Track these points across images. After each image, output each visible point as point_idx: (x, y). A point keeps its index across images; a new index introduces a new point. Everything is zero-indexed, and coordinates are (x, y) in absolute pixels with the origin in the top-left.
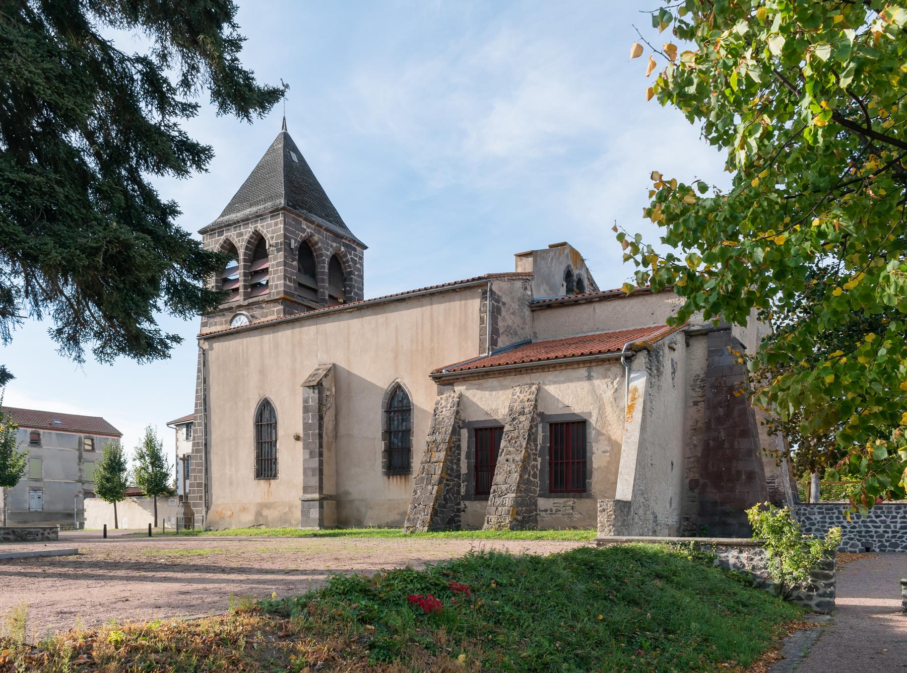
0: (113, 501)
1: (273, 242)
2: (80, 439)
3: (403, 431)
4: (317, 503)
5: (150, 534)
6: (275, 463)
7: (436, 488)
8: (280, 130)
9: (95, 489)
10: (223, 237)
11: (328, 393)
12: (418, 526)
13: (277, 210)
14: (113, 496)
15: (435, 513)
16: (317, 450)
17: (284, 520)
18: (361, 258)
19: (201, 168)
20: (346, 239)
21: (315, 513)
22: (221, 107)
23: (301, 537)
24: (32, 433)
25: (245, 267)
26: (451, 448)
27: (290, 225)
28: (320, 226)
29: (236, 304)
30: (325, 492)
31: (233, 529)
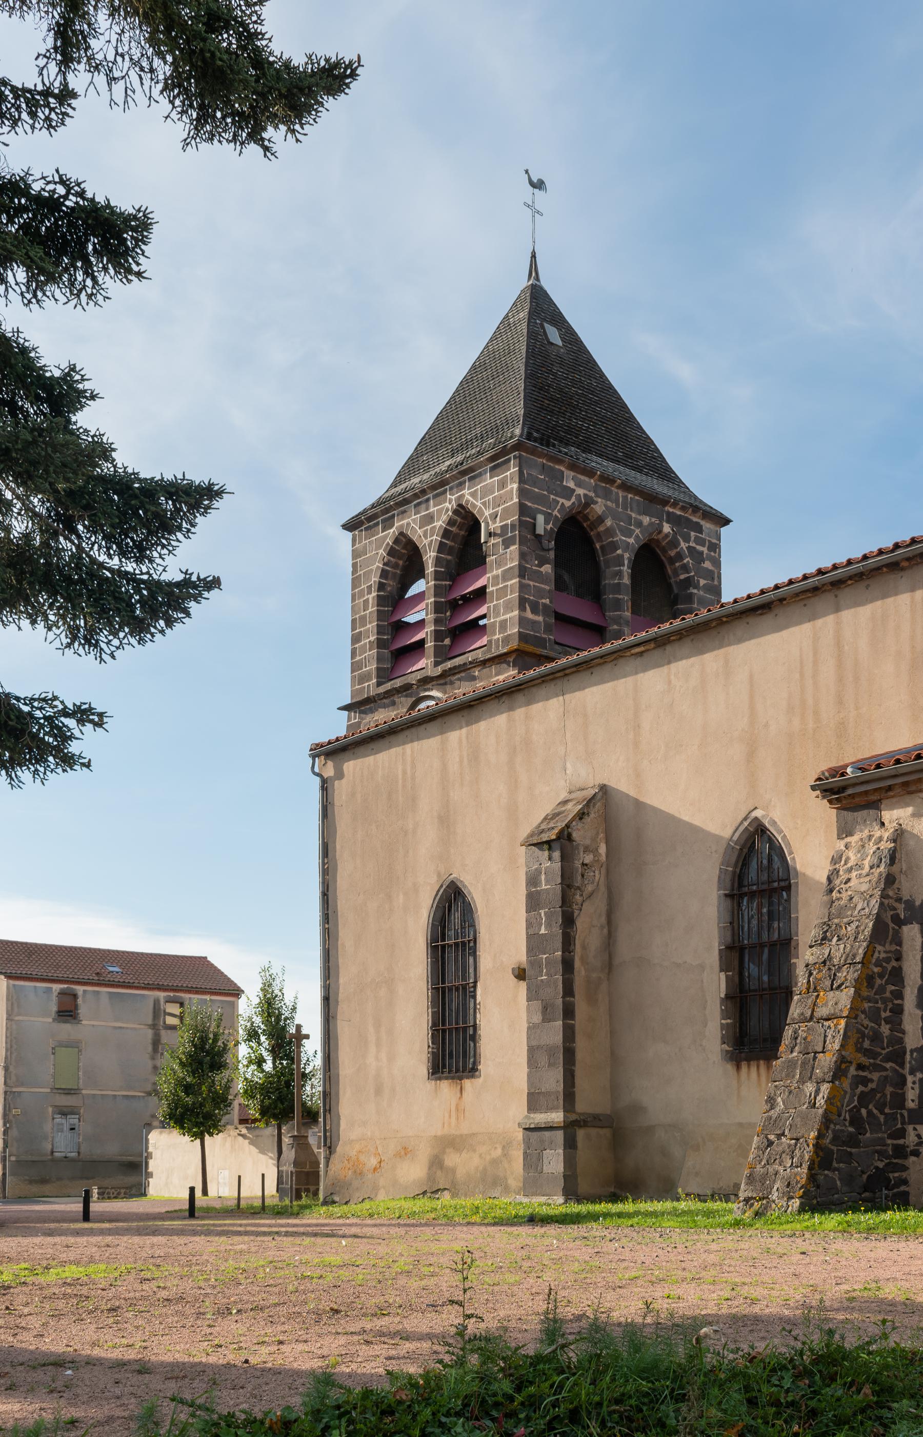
0: (200, 1136)
1: (495, 526)
2: (156, 1002)
3: (773, 945)
4: (559, 1135)
5: (192, 1211)
6: (474, 1038)
7: (825, 1088)
8: (523, 282)
9: (162, 1109)
10: (392, 531)
11: (589, 854)
12: (775, 1195)
13: (504, 452)
14: (197, 1125)
15: (822, 1159)
16: (559, 1002)
17: (491, 1180)
18: (715, 547)
19: (129, 271)
20: (675, 505)
21: (554, 1162)
22: (199, 124)
23: (499, 1222)
24: (62, 993)
25: (438, 591)
26: (870, 979)
27: (535, 482)
28: (607, 479)
29: (419, 676)
30: (581, 1106)
31: (382, 1201)
